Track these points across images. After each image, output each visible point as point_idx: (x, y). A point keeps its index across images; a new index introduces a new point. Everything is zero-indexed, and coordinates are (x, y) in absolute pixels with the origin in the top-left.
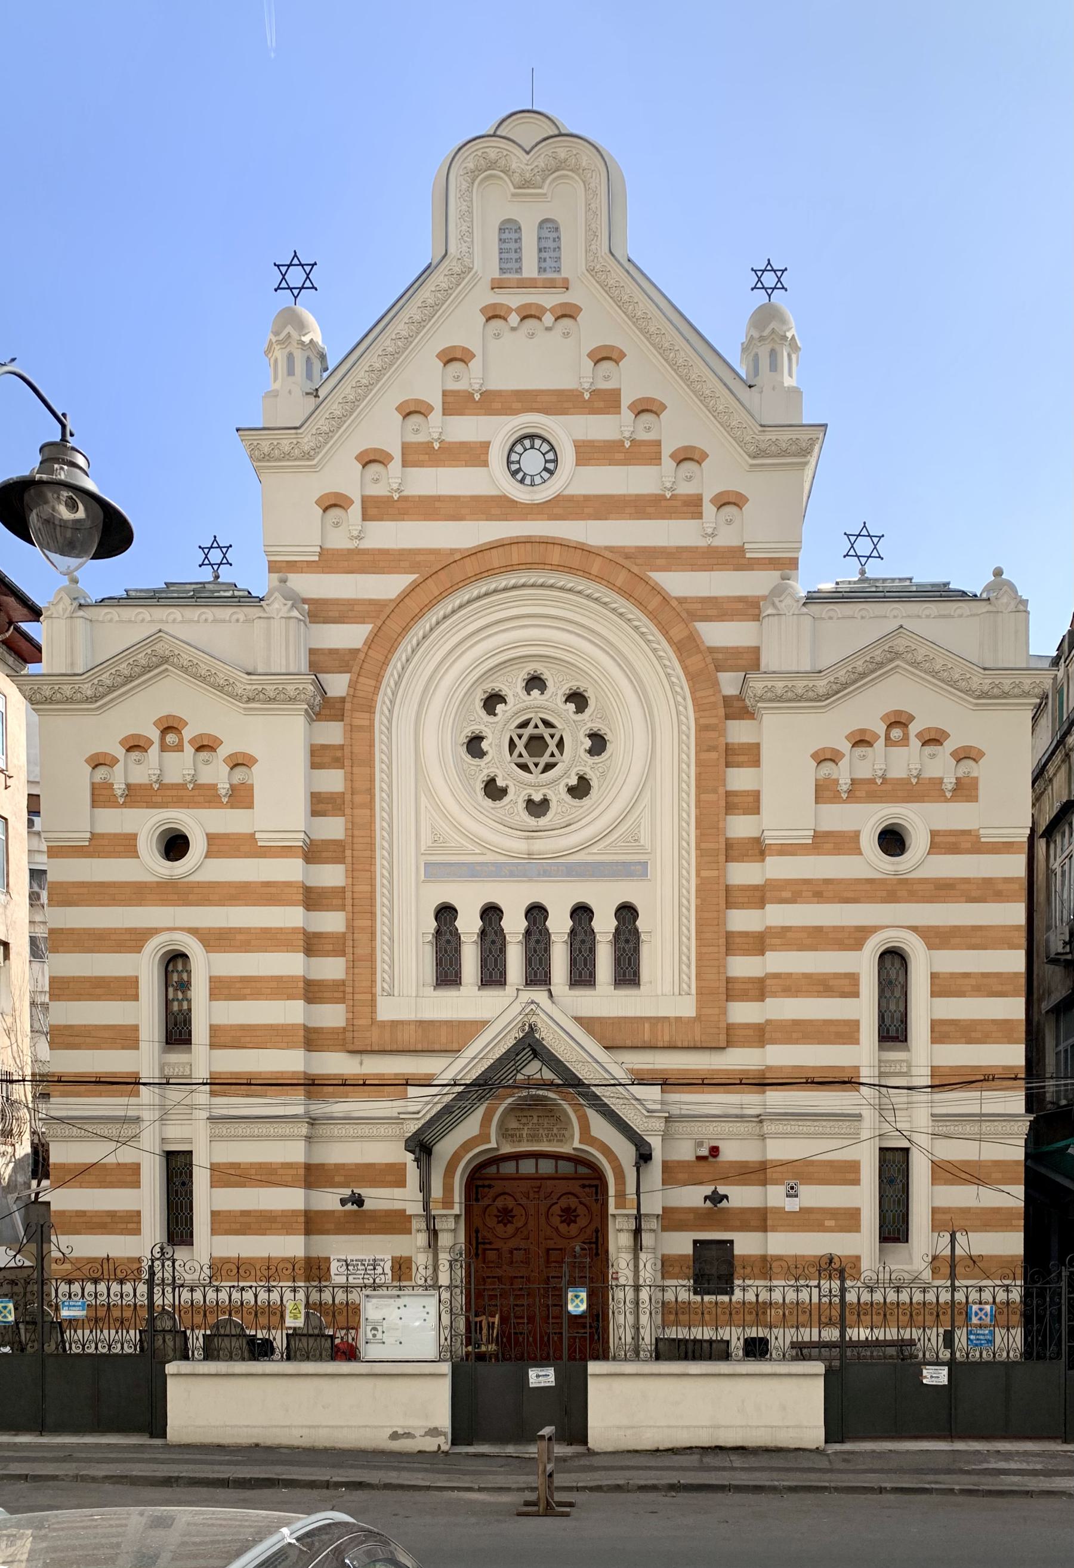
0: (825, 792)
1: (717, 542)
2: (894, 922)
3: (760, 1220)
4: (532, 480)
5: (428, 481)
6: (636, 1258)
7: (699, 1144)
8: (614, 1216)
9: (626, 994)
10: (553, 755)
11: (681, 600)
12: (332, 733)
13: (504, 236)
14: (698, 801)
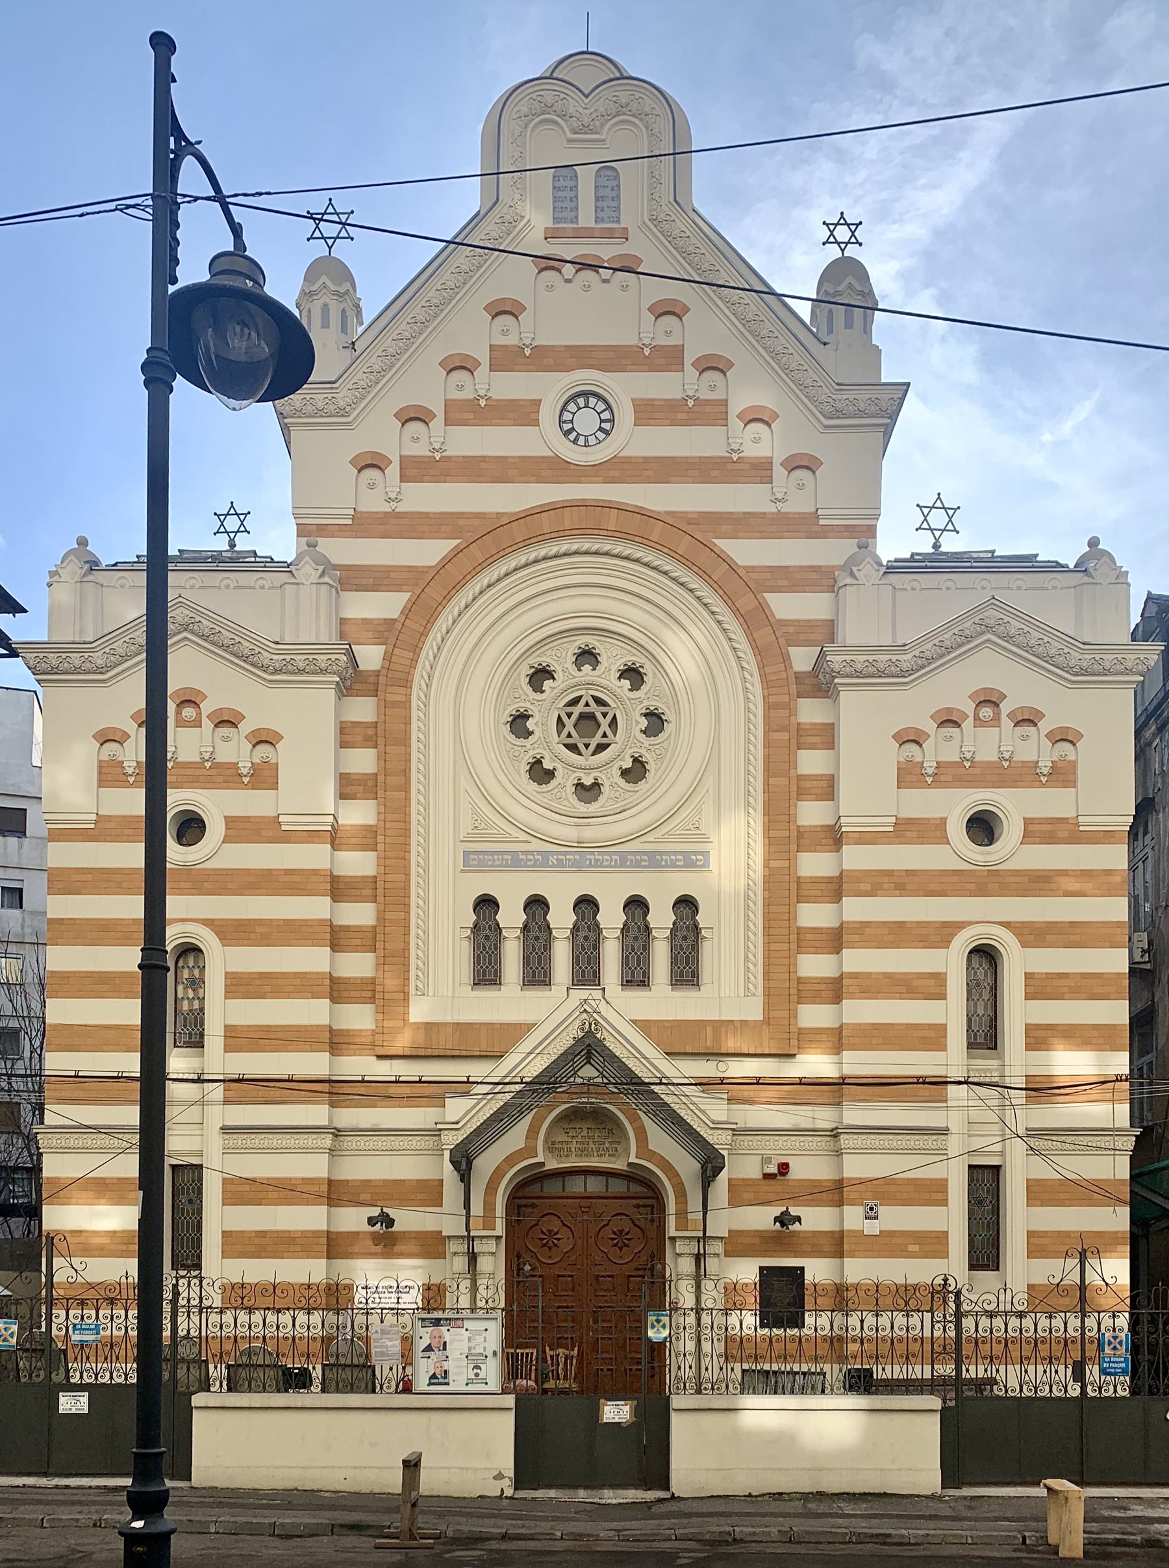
0: (909, 776)
1: (786, 508)
2: (985, 917)
3: (836, 1245)
4: (587, 441)
5: (469, 441)
6: (698, 1287)
7: (766, 1160)
8: (673, 1239)
9: (685, 995)
10: (605, 735)
11: (751, 569)
12: (363, 710)
13: (557, 184)
14: (767, 784)
